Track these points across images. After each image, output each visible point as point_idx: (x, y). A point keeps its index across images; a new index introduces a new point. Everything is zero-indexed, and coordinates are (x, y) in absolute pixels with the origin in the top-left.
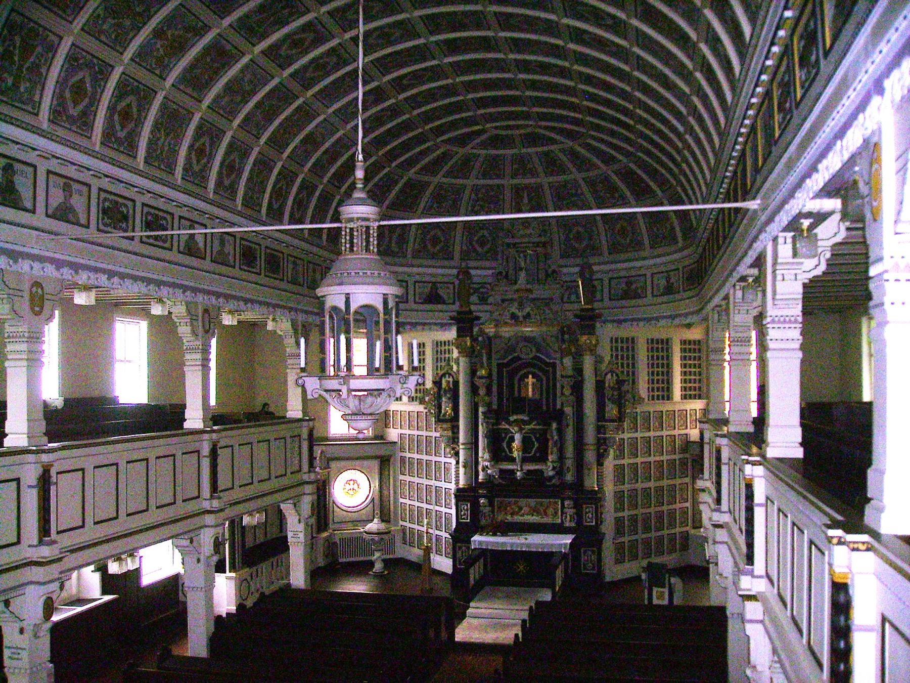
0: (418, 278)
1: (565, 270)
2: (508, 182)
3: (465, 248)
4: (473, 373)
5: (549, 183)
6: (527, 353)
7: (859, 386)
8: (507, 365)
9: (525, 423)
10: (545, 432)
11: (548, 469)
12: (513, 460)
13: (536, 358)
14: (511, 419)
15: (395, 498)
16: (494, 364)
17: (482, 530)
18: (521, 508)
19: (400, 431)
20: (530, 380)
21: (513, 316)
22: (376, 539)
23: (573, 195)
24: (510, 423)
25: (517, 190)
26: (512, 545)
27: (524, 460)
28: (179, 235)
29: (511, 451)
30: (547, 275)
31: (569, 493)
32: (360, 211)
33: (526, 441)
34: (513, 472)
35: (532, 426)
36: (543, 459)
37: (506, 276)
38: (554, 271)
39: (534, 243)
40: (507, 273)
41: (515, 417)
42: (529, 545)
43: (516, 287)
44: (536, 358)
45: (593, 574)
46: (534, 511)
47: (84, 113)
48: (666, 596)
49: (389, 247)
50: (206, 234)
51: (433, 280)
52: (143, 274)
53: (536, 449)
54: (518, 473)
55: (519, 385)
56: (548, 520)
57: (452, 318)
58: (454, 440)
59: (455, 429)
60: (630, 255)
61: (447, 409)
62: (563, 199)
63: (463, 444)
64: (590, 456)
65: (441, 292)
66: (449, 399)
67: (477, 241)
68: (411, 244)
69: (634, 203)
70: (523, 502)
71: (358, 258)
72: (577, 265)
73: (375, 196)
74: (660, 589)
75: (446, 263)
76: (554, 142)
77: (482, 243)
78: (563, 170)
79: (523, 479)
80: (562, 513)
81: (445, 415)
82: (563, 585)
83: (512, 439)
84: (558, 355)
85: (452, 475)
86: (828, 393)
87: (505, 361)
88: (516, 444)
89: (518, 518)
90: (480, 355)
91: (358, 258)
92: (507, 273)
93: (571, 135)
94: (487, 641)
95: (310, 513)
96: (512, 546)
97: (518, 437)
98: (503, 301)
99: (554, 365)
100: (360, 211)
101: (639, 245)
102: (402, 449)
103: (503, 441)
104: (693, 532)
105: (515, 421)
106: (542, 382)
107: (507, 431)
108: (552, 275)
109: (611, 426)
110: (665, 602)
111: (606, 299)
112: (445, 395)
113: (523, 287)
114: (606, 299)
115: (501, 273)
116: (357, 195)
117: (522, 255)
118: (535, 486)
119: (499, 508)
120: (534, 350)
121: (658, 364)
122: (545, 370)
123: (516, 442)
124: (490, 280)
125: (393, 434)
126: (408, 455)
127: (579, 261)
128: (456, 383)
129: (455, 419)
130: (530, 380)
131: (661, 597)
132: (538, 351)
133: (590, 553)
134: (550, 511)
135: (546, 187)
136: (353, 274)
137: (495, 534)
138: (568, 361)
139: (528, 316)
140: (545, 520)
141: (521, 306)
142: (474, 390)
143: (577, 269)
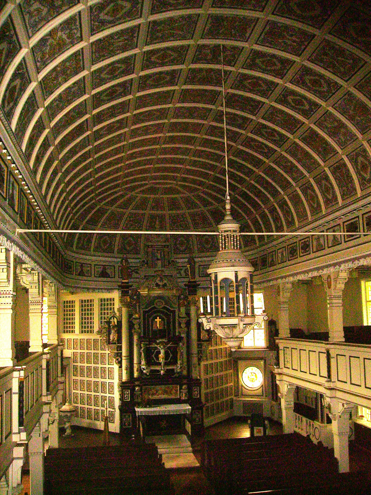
0: (96, 263)
1: (179, 260)
2: (148, 212)
3: (120, 247)
4: (130, 316)
5: (169, 214)
6: (160, 306)
7: (362, 320)
8: (147, 312)
9: (167, 343)
10: (175, 348)
11: (177, 368)
12: (160, 364)
13: (164, 308)
14: (158, 341)
15: (69, 390)
16: (142, 312)
17: (139, 405)
18: (157, 391)
19: (73, 351)
20: (158, 320)
21: (157, 285)
22: (69, 415)
23: (181, 221)
24: (158, 344)
25: (153, 218)
26: (159, 412)
27: (166, 364)
28: (327, 235)
29: (158, 358)
30: (169, 263)
31: (185, 381)
32: (229, 226)
33: (166, 353)
34: (158, 371)
35: (169, 345)
36: (175, 363)
37: (147, 263)
38: (173, 261)
39: (162, 246)
40: (147, 261)
41: (160, 340)
42: (169, 411)
43: (156, 269)
44: (164, 308)
45: (199, 425)
46: (166, 392)
47: (356, 162)
48: (262, 432)
49: (83, 244)
50: (341, 235)
51: (104, 264)
52: (350, 258)
53: (172, 358)
54: (162, 372)
55: (152, 322)
56: (173, 397)
57: (119, 286)
58: (119, 355)
59: (120, 348)
60: (209, 254)
61: (113, 336)
62: (177, 223)
63: (125, 356)
64: (195, 360)
65: (108, 271)
66: (116, 331)
67: (127, 243)
68: (93, 244)
69: (192, 228)
70: (158, 387)
71: (228, 252)
72: (120, 258)
73: (236, 216)
74: (257, 428)
75: (109, 255)
76: (178, 192)
77: (129, 244)
78: (178, 208)
79: (164, 374)
80: (180, 392)
81: (113, 340)
82: (192, 432)
83: (159, 353)
84: (177, 306)
85: (116, 375)
86: (352, 324)
87: (147, 310)
88: (162, 355)
89: (156, 397)
90: (135, 306)
91: (228, 252)
92: (147, 261)
93: (191, 190)
94: (173, 467)
95: (61, 401)
96: (141, 413)
97: (162, 351)
98: (145, 276)
99: (174, 312)
100: (229, 226)
101: (88, 249)
102: (75, 361)
103: (153, 355)
104: (235, 398)
105: (160, 342)
106: (164, 320)
107: (156, 348)
108: (172, 263)
109: (205, 344)
110: (261, 434)
111: (93, 276)
112: (113, 329)
113: (160, 269)
114: (93, 276)
115: (143, 261)
116: (228, 218)
117: (159, 252)
118: (170, 378)
119: (145, 392)
120: (164, 303)
121: (105, 313)
122: (168, 315)
123: (161, 354)
124: (138, 265)
125: (68, 353)
126: (79, 364)
127: (188, 255)
128: (120, 323)
129: (119, 340)
130: (158, 320)
131: (259, 431)
132: (166, 304)
133: (197, 413)
134: (173, 391)
135: (167, 217)
136: (237, 260)
137: (146, 407)
138: (183, 310)
139: (165, 285)
140: (170, 397)
141: (161, 280)
142: (131, 326)
143: (186, 260)
